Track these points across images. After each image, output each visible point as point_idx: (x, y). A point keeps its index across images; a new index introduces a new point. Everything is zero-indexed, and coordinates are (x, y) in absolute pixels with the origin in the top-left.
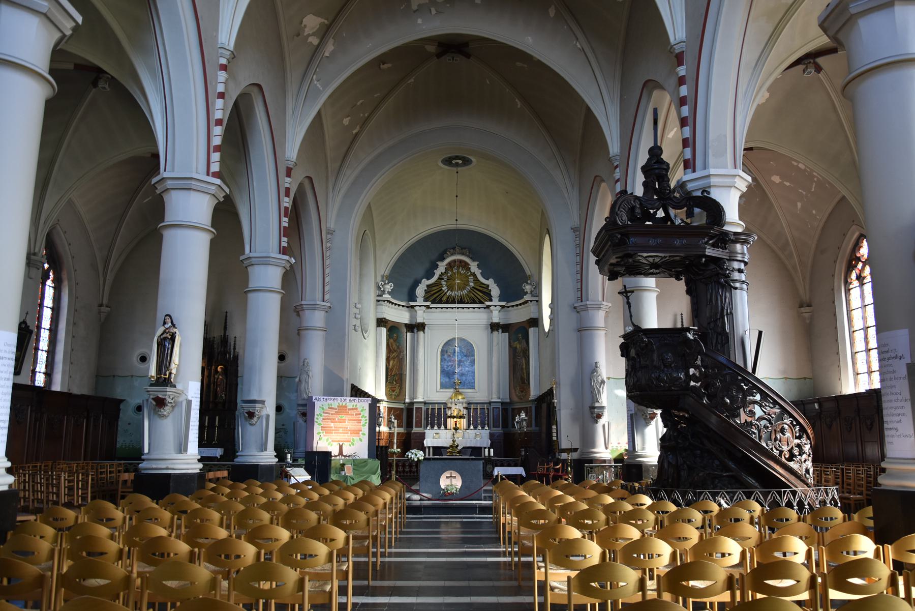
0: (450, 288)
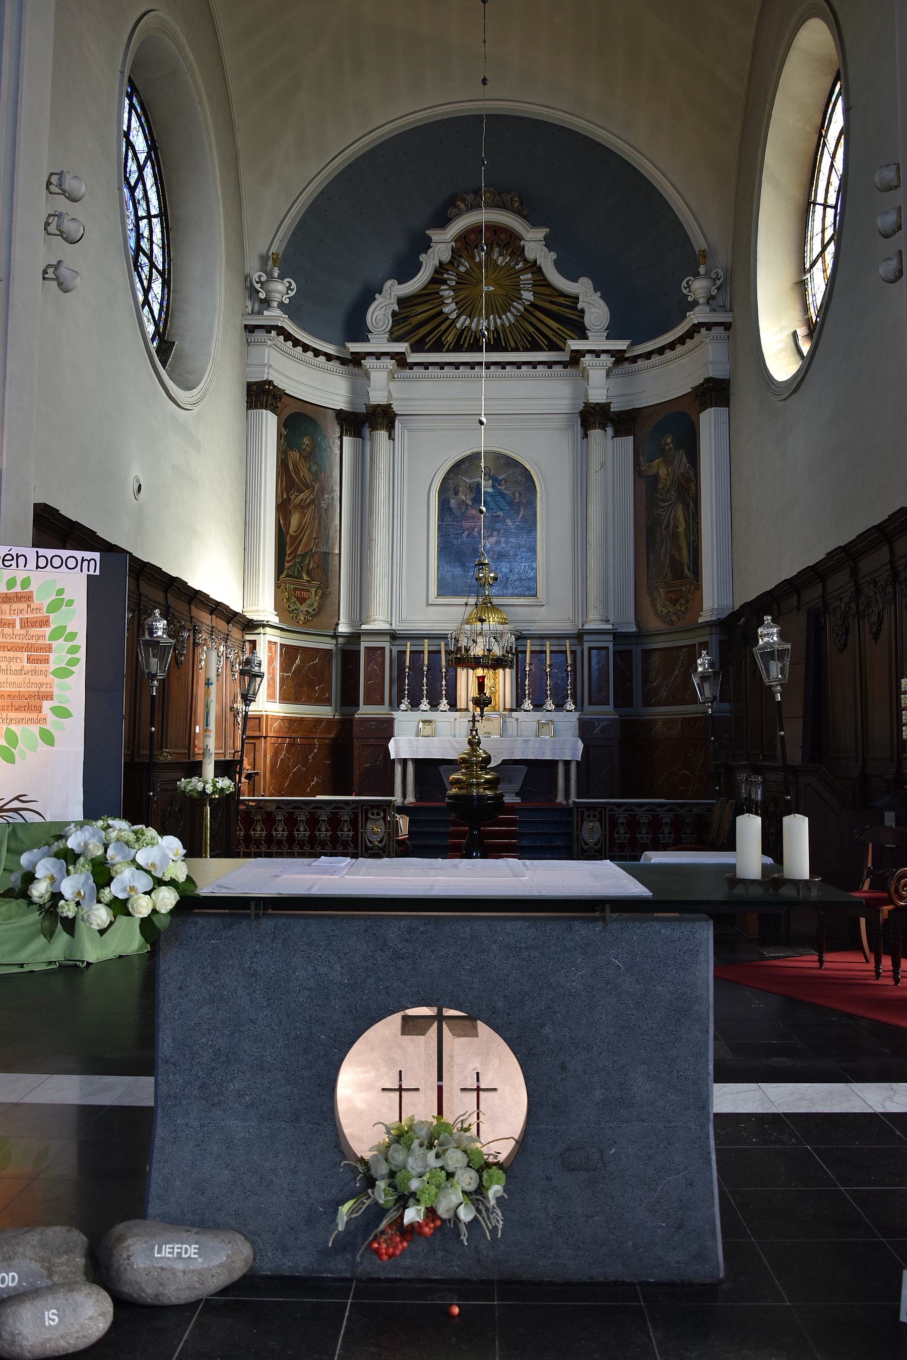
0: (467, 307)
